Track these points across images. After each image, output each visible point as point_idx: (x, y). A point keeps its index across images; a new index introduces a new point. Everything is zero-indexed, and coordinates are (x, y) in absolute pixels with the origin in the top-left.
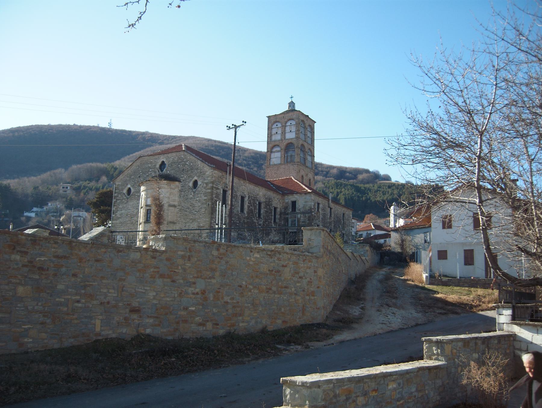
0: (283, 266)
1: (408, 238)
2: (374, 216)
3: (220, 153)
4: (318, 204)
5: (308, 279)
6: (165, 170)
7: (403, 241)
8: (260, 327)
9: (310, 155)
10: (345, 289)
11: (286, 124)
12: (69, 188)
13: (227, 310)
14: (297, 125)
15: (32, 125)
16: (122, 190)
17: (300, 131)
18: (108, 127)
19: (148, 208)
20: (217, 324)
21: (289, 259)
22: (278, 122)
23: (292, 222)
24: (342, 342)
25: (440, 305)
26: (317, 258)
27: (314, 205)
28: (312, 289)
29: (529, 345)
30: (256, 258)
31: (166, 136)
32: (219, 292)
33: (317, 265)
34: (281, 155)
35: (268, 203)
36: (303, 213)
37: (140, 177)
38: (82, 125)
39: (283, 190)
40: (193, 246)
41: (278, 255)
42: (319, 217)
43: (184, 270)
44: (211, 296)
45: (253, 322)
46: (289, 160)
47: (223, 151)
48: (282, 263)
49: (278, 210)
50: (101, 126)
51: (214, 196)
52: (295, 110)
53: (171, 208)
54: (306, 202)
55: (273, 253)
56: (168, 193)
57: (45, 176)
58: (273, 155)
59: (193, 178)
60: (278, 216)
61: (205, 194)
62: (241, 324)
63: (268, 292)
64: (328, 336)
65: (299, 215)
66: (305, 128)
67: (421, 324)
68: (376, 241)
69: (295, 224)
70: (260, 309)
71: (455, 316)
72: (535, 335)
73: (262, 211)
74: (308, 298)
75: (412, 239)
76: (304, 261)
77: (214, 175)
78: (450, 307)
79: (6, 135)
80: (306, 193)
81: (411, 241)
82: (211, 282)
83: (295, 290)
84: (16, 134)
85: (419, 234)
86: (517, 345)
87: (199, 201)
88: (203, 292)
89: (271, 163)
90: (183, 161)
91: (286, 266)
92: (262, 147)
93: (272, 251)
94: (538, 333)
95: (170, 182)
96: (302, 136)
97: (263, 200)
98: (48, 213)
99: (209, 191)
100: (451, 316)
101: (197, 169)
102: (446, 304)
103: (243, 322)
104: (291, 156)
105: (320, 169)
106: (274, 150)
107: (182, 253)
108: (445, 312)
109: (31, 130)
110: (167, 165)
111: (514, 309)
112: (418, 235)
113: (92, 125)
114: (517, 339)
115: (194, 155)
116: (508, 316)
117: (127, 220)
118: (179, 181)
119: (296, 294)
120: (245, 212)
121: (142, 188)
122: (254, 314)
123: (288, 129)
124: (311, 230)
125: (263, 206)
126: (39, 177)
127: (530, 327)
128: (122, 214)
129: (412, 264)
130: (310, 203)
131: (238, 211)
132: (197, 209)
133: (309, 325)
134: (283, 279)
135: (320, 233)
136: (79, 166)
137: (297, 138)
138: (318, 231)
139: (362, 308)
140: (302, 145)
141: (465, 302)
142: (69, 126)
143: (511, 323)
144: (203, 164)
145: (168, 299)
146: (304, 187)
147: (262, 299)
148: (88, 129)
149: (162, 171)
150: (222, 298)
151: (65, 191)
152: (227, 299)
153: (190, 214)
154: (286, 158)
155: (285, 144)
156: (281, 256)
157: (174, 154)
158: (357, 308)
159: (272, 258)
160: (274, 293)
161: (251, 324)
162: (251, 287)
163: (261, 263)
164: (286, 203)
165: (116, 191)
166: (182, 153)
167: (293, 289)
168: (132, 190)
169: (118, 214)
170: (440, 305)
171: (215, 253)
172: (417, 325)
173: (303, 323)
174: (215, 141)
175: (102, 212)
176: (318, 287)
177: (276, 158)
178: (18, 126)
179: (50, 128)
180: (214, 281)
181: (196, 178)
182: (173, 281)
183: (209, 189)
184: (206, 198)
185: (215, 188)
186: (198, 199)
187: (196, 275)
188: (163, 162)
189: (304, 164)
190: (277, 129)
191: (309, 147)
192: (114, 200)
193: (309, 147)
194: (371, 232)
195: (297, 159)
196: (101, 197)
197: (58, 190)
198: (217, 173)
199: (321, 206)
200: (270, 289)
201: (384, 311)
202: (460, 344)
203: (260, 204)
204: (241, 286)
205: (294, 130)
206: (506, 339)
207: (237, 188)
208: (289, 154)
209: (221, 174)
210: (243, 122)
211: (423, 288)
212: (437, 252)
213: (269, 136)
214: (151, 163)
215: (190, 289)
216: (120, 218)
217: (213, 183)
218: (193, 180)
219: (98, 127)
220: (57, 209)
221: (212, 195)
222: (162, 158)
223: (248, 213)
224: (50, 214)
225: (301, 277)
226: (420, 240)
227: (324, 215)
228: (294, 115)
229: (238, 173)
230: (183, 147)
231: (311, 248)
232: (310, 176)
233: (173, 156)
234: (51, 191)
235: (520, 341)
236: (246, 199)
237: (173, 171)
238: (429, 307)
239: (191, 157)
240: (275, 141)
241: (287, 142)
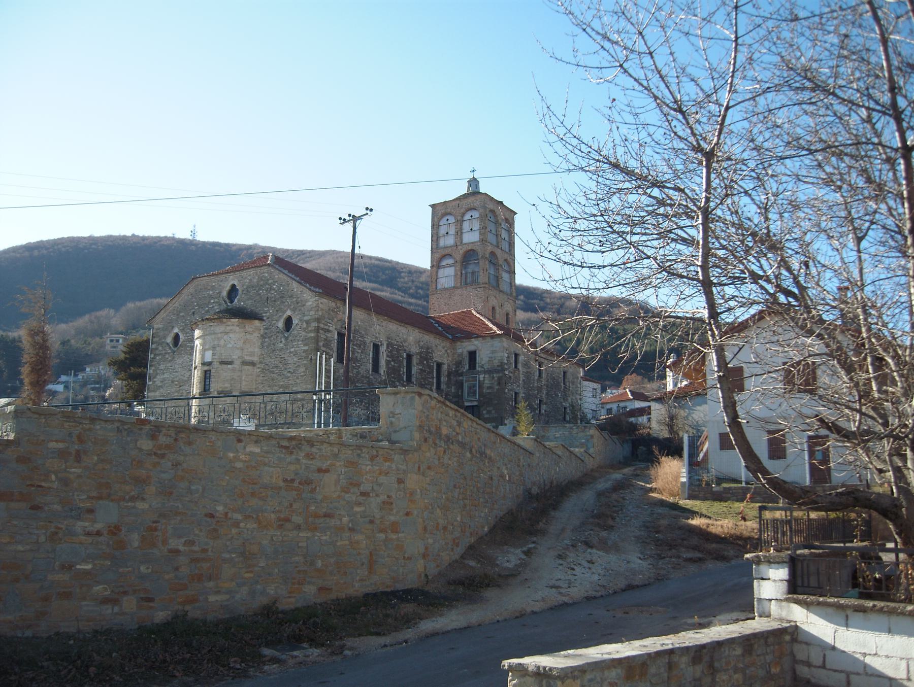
0: (320, 470)
1: (682, 412)
2: (639, 378)
3: (378, 277)
4: (516, 355)
5: (383, 497)
6: (236, 300)
7: (672, 418)
8: (262, 600)
9: (506, 271)
10: (510, 513)
11: (462, 217)
12: (121, 341)
13: (177, 569)
14: (482, 218)
15: (63, 238)
16: (165, 338)
17: (488, 229)
18: (191, 238)
19: (206, 368)
20: (151, 600)
21: (336, 456)
22: (450, 214)
23: (470, 388)
24: (434, 634)
25: (695, 541)
26: (405, 452)
27: (508, 357)
28: (392, 518)
29: (828, 653)
30: (252, 454)
31: (288, 250)
32: (156, 529)
33: (404, 467)
34: (456, 271)
35: (426, 355)
36: (489, 372)
37: (194, 313)
38: (146, 235)
39: (454, 332)
40: (90, 430)
41: (306, 448)
42: (517, 378)
43: (65, 482)
44: (135, 540)
45: (245, 590)
46: (469, 280)
47: (383, 273)
48: (317, 463)
49: (445, 368)
50: (177, 236)
51: (321, 344)
52: (479, 193)
53: (246, 367)
54: (493, 352)
55: (294, 443)
56: (238, 339)
57: (82, 322)
58: (441, 272)
59: (285, 312)
60: (444, 379)
61: (306, 341)
62: (212, 598)
63: (280, 527)
64: (408, 621)
65: (482, 376)
66: (497, 223)
67: (638, 586)
68: (632, 419)
69: (475, 392)
70: (262, 564)
71: (720, 565)
72: (842, 630)
73: (414, 370)
74: (382, 536)
75: (689, 414)
76: (372, 459)
77: (321, 306)
78: (714, 545)
79: (18, 255)
80: (494, 336)
81: (686, 418)
82: (134, 507)
83: (351, 521)
84: (36, 253)
85: (700, 405)
86: (801, 653)
87: (295, 353)
88: (114, 530)
89: (439, 287)
90: (267, 284)
91: (327, 471)
92: (421, 259)
93: (291, 439)
94: (847, 626)
95: (245, 321)
96: (491, 238)
97: (414, 350)
98: (85, 384)
99: (312, 335)
100: (710, 565)
101: (291, 297)
102: (707, 540)
103: (218, 592)
104: (473, 273)
105: (548, 300)
106: (444, 263)
107: (61, 445)
108: (700, 555)
109: (60, 246)
110: (240, 292)
111: (793, 563)
112: (698, 408)
113: (162, 235)
114: (800, 638)
115: (286, 272)
116: (780, 584)
117: (173, 390)
118: (261, 319)
119: (351, 530)
120: (383, 369)
121: (197, 333)
122: (247, 575)
123: (466, 226)
124: (395, 394)
125: (415, 360)
126: (71, 324)
127: (830, 610)
128: (164, 380)
129: (663, 458)
130: (501, 354)
131: (367, 371)
132: (292, 368)
133: (383, 593)
134: (320, 497)
135: (413, 399)
136: (138, 304)
137: (483, 241)
138: (409, 396)
139: (528, 553)
140: (493, 254)
141: (746, 534)
142: (124, 238)
143: (787, 600)
144: (301, 288)
145: (20, 548)
146: (491, 325)
147: (265, 542)
148: (155, 243)
149: (232, 302)
150: (165, 542)
151: (114, 347)
152: (174, 543)
153: (279, 378)
154: (464, 276)
155: (461, 252)
156: (314, 450)
157: (252, 272)
158: (518, 551)
159: (292, 453)
160: (298, 527)
161: (238, 597)
162: (239, 516)
163: (265, 464)
164: (459, 355)
165: (155, 340)
166: (265, 269)
167: (345, 520)
168: (182, 337)
169: (158, 380)
170: (695, 541)
171: (146, 444)
172: (630, 587)
173: (370, 590)
174: (370, 258)
175: (133, 377)
176: (407, 514)
177: (448, 276)
178: (38, 240)
179: (92, 241)
180: (141, 505)
181: (289, 313)
182: (35, 508)
183: (311, 331)
184: (306, 348)
185: (322, 329)
186: (292, 350)
187: (94, 494)
188: (233, 286)
189: (497, 287)
190: (448, 226)
191: (506, 256)
192: (151, 356)
193: (506, 256)
194: (627, 404)
195: (483, 278)
196: (132, 352)
197: (103, 346)
198: (326, 303)
199: (521, 358)
200: (288, 520)
201: (572, 556)
202: (613, 674)
203: (409, 357)
204: (212, 516)
205: (477, 228)
206: (771, 640)
207: (366, 329)
208: (470, 270)
209: (333, 304)
210: (367, 209)
211: (675, 507)
212: (717, 437)
213: (435, 239)
214: (213, 288)
215: (80, 523)
216: (161, 387)
217: (318, 320)
218: (285, 316)
219: (173, 238)
220: (99, 376)
221: (317, 342)
222: (232, 280)
223: (388, 373)
224: (89, 386)
225: (363, 494)
226: (702, 415)
227: (528, 375)
228: (475, 201)
229: (360, 300)
230: (270, 258)
231: (395, 432)
232: (508, 307)
233: (250, 275)
234: (90, 347)
235: (807, 644)
236: (383, 349)
237: (249, 302)
238: (671, 546)
239: (282, 276)
240: (446, 247)
241: (465, 248)
